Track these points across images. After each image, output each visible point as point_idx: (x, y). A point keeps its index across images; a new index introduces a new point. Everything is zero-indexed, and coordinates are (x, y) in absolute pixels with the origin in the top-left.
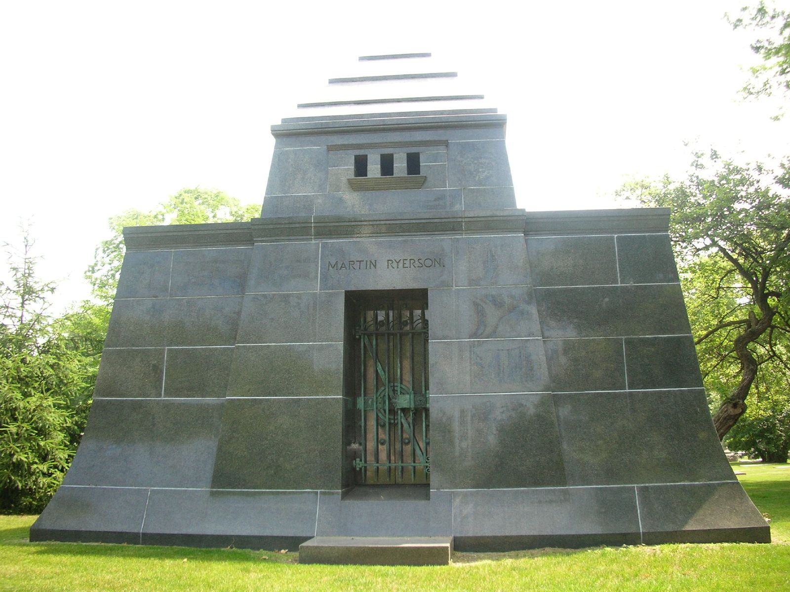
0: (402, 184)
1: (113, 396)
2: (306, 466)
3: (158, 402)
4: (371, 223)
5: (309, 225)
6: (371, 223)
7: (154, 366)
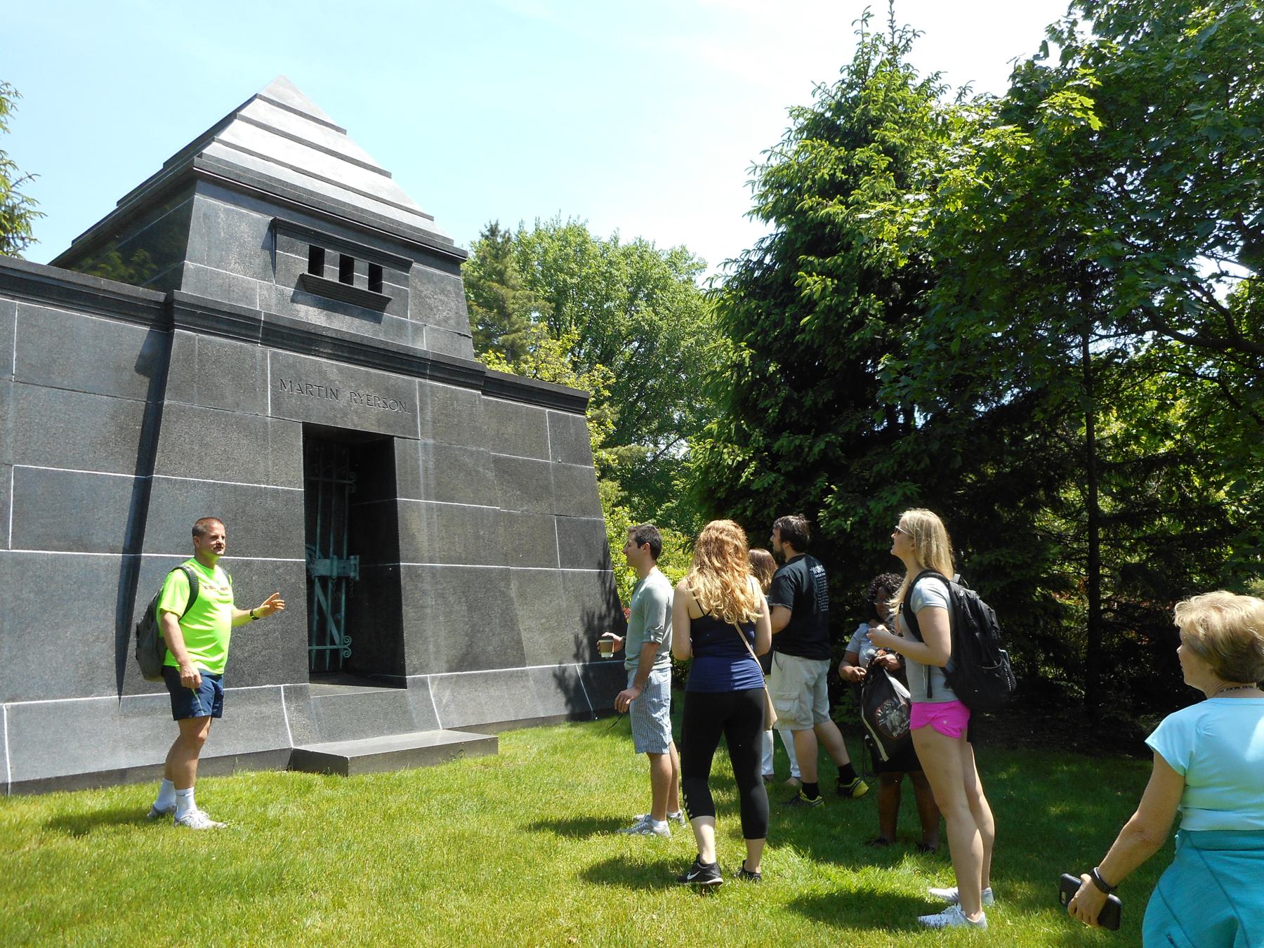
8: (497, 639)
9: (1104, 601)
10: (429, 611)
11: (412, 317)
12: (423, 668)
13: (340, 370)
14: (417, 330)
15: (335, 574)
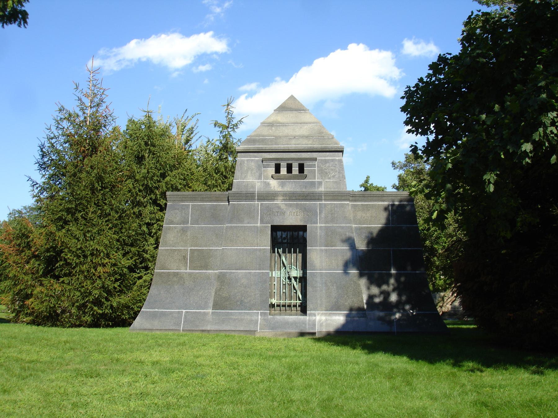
0: (295, 177)
1: (165, 270)
2: (254, 301)
3: (186, 273)
4: (282, 195)
5: (255, 195)
6: (282, 195)
7: (184, 256)
8: (350, 300)
9: (96, 314)
10: (318, 288)
11: (317, 179)
12: (315, 309)
13: (286, 204)
14: (320, 183)
15: (298, 276)
